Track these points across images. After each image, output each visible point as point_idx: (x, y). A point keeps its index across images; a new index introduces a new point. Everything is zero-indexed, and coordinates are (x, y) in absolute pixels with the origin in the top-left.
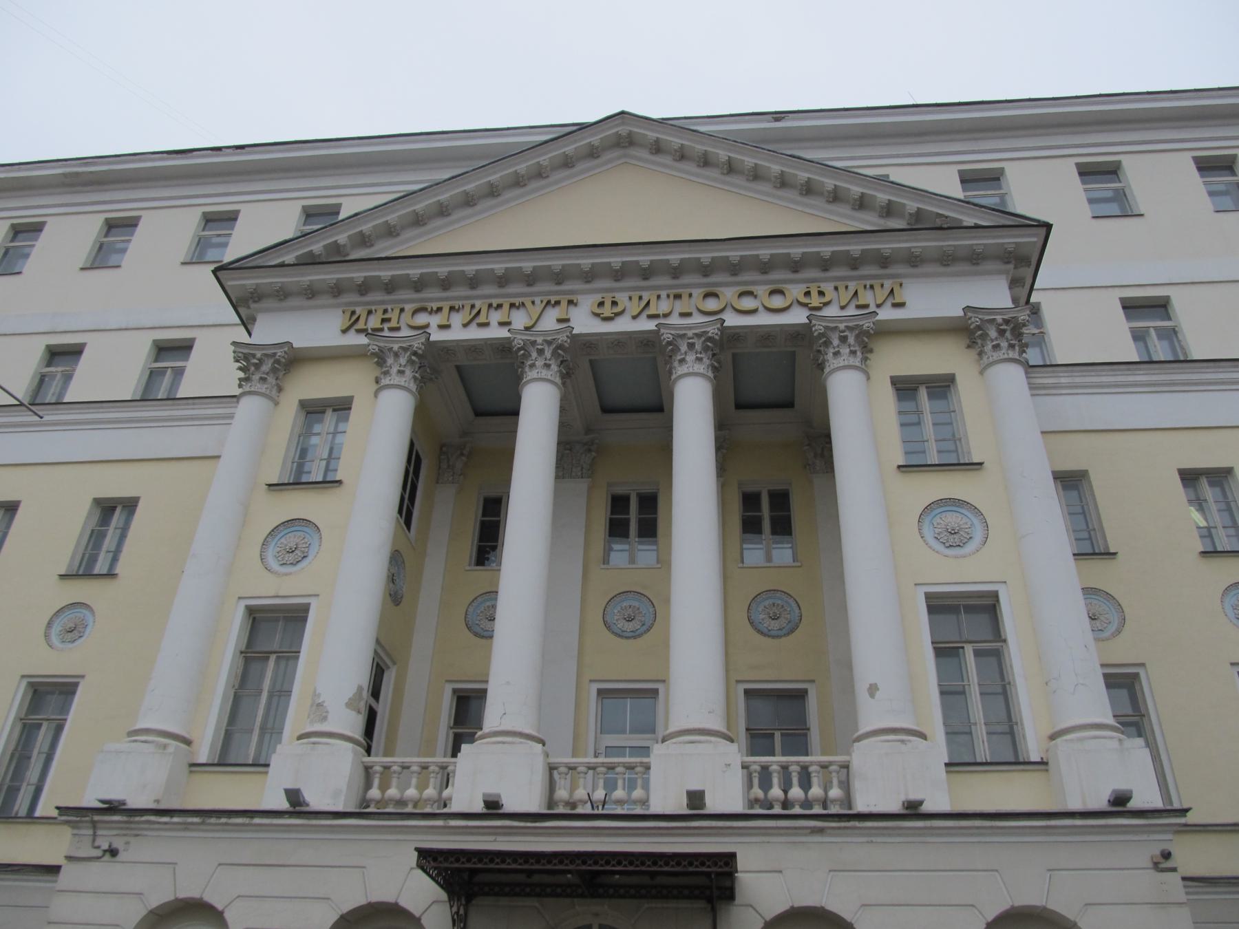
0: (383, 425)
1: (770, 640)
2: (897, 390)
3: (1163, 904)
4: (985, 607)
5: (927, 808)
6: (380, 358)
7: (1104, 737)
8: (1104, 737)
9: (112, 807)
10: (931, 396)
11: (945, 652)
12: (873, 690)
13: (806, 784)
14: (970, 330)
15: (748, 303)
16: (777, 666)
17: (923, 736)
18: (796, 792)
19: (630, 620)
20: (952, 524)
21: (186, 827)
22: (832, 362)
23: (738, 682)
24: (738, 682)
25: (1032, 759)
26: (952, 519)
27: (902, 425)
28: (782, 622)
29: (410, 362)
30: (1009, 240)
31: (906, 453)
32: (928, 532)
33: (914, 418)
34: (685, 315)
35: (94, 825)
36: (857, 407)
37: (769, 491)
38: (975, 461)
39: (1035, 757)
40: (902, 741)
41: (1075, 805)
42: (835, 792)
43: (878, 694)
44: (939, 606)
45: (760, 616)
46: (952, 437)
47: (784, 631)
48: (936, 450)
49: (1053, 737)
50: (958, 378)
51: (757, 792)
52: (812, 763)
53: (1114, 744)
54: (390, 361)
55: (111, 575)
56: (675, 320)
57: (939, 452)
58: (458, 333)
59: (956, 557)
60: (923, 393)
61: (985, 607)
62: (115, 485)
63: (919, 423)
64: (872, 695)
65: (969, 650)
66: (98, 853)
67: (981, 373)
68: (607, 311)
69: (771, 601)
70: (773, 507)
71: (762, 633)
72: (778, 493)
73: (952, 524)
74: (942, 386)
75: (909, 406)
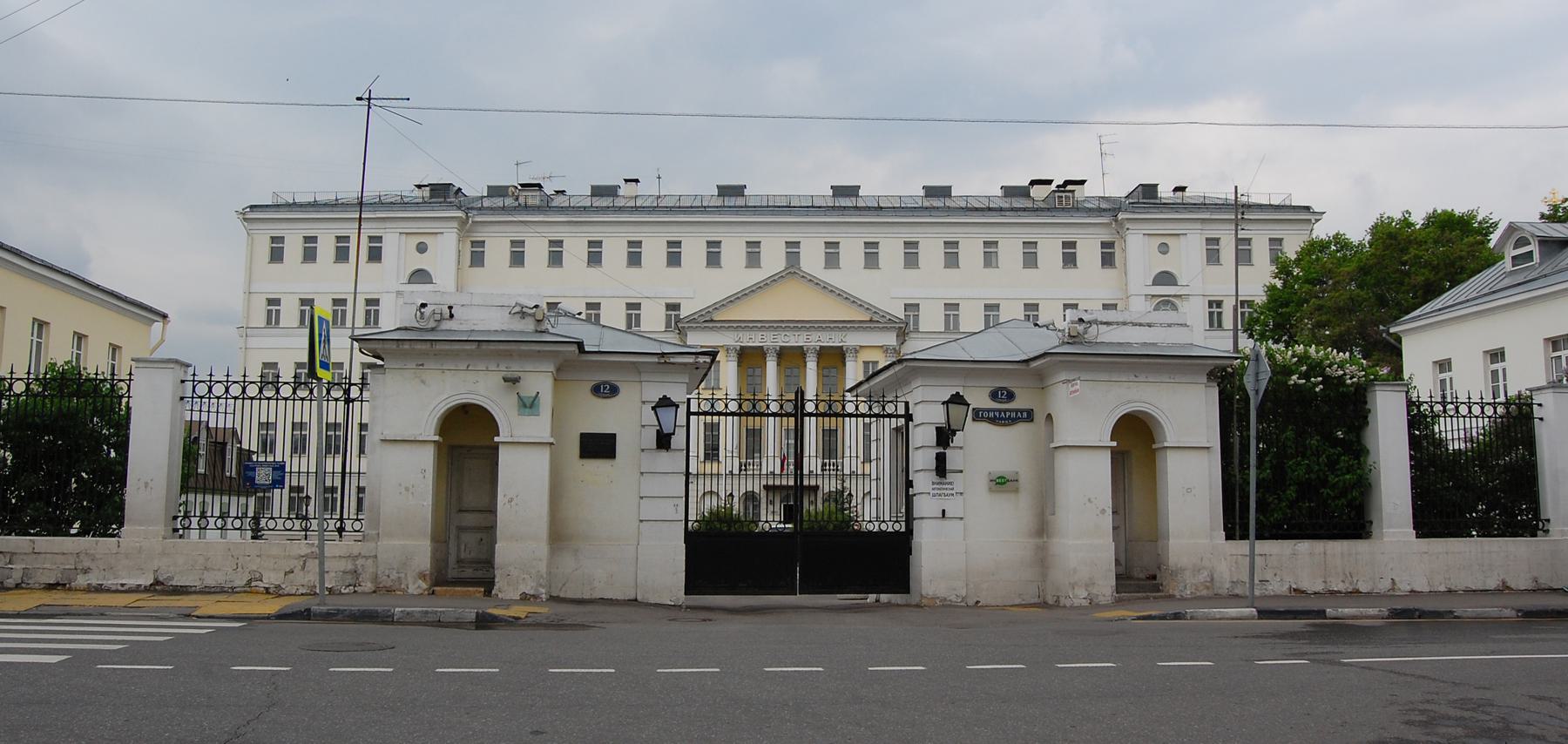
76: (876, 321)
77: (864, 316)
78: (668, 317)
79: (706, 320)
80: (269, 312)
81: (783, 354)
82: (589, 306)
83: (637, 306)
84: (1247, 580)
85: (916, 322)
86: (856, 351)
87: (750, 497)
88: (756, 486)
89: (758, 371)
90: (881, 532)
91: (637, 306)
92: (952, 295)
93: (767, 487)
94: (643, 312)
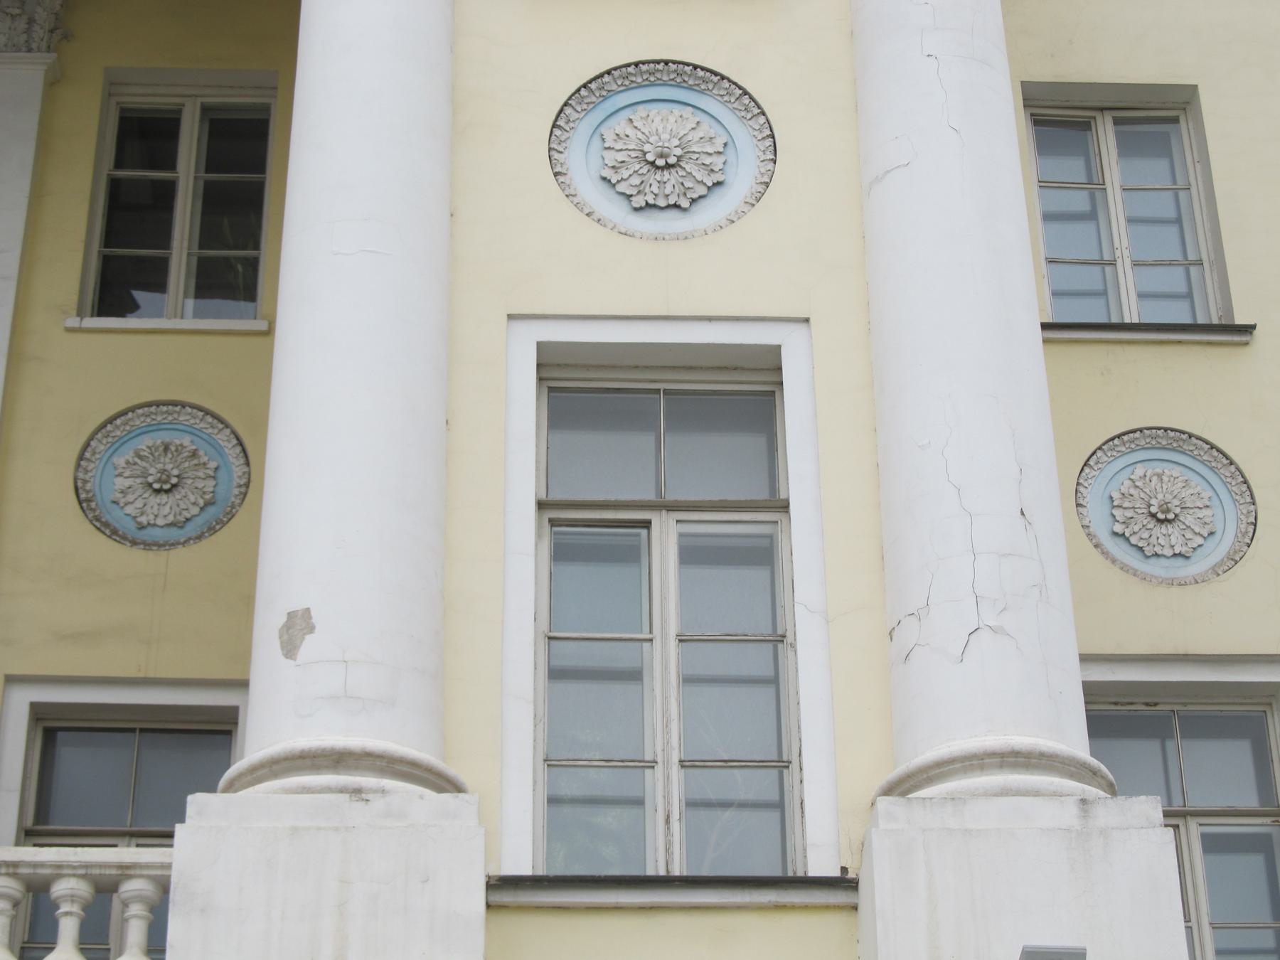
1: (137, 556)
4: (735, 394)
7: (1036, 793)
8: (1036, 793)
10: (1126, 148)
11: (585, 534)
12: (297, 627)
23: (11, 680)
24: (11, 680)
25: (813, 872)
26: (664, 124)
27: (1048, 217)
28: (186, 501)
31: (1056, 294)
32: (583, 162)
33: (1079, 201)
37: (205, 109)
38: (1239, 320)
39: (821, 865)
40: (357, 792)
43: (309, 647)
44: (583, 390)
45: (116, 480)
46: (1199, 259)
47: (190, 529)
50: (1207, 100)
52: (60, 870)
53: (1067, 814)
57: (1142, 296)
59: (1171, 582)
60: (1106, 134)
61: (735, 394)
63: (1091, 216)
64: (290, 648)
65: (666, 536)
69: (158, 438)
70: (213, 161)
71: (114, 533)
75: (1072, 168)
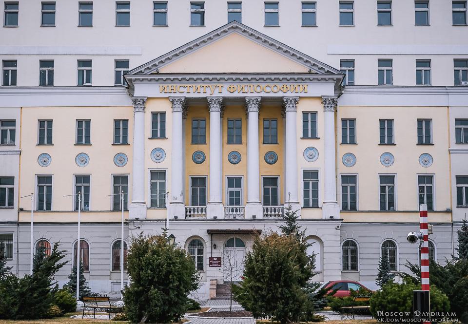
0: (175, 121)
2: (304, 114)
3: (336, 235)
5: (335, 218)
6: (173, 102)
9: (137, 219)
13: (275, 211)
14: (324, 100)
15: (268, 89)
16: (271, 171)
17: (298, 203)
18: (273, 213)
19: (235, 159)
20: (311, 154)
21: (153, 223)
22: (288, 109)
26: (311, 152)
29: (180, 103)
30: (335, 77)
34: (253, 92)
35: (134, 223)
36: (294, 121)
41: (324, 218)
42: (281, 213)
48: (310, 130)
49: (324, 203)
51: (265, 213)
54: (175, 103)
55: (210, 266)
56: (249, 95)
58: (193, 95)
62: (84, 116)
66: (136, 228)
67: (324, 111)
68: (232, 90)
72: (272, 132)
73: (311, 154)
74: (314, 114)
76: (317, 72)
77: (302, 68)
78: (118, 73)
79: (152, 72)
80: (6, 73)
81: (226, 105)
82: (343, 62)
83: (88, 63)
84: (207, 219)
85: (352, 78)
86: (296, 102)
87: (195, 242)
88: (200, 230)
89: (202, 123)
90: (281, 276)
91: (88, 63)
92: (386, 51)
93: (211, 233)
94: (19, 69)
